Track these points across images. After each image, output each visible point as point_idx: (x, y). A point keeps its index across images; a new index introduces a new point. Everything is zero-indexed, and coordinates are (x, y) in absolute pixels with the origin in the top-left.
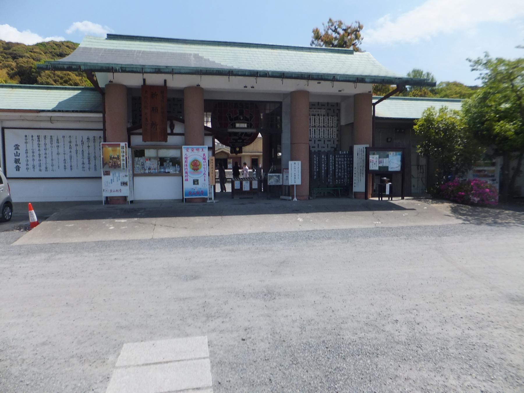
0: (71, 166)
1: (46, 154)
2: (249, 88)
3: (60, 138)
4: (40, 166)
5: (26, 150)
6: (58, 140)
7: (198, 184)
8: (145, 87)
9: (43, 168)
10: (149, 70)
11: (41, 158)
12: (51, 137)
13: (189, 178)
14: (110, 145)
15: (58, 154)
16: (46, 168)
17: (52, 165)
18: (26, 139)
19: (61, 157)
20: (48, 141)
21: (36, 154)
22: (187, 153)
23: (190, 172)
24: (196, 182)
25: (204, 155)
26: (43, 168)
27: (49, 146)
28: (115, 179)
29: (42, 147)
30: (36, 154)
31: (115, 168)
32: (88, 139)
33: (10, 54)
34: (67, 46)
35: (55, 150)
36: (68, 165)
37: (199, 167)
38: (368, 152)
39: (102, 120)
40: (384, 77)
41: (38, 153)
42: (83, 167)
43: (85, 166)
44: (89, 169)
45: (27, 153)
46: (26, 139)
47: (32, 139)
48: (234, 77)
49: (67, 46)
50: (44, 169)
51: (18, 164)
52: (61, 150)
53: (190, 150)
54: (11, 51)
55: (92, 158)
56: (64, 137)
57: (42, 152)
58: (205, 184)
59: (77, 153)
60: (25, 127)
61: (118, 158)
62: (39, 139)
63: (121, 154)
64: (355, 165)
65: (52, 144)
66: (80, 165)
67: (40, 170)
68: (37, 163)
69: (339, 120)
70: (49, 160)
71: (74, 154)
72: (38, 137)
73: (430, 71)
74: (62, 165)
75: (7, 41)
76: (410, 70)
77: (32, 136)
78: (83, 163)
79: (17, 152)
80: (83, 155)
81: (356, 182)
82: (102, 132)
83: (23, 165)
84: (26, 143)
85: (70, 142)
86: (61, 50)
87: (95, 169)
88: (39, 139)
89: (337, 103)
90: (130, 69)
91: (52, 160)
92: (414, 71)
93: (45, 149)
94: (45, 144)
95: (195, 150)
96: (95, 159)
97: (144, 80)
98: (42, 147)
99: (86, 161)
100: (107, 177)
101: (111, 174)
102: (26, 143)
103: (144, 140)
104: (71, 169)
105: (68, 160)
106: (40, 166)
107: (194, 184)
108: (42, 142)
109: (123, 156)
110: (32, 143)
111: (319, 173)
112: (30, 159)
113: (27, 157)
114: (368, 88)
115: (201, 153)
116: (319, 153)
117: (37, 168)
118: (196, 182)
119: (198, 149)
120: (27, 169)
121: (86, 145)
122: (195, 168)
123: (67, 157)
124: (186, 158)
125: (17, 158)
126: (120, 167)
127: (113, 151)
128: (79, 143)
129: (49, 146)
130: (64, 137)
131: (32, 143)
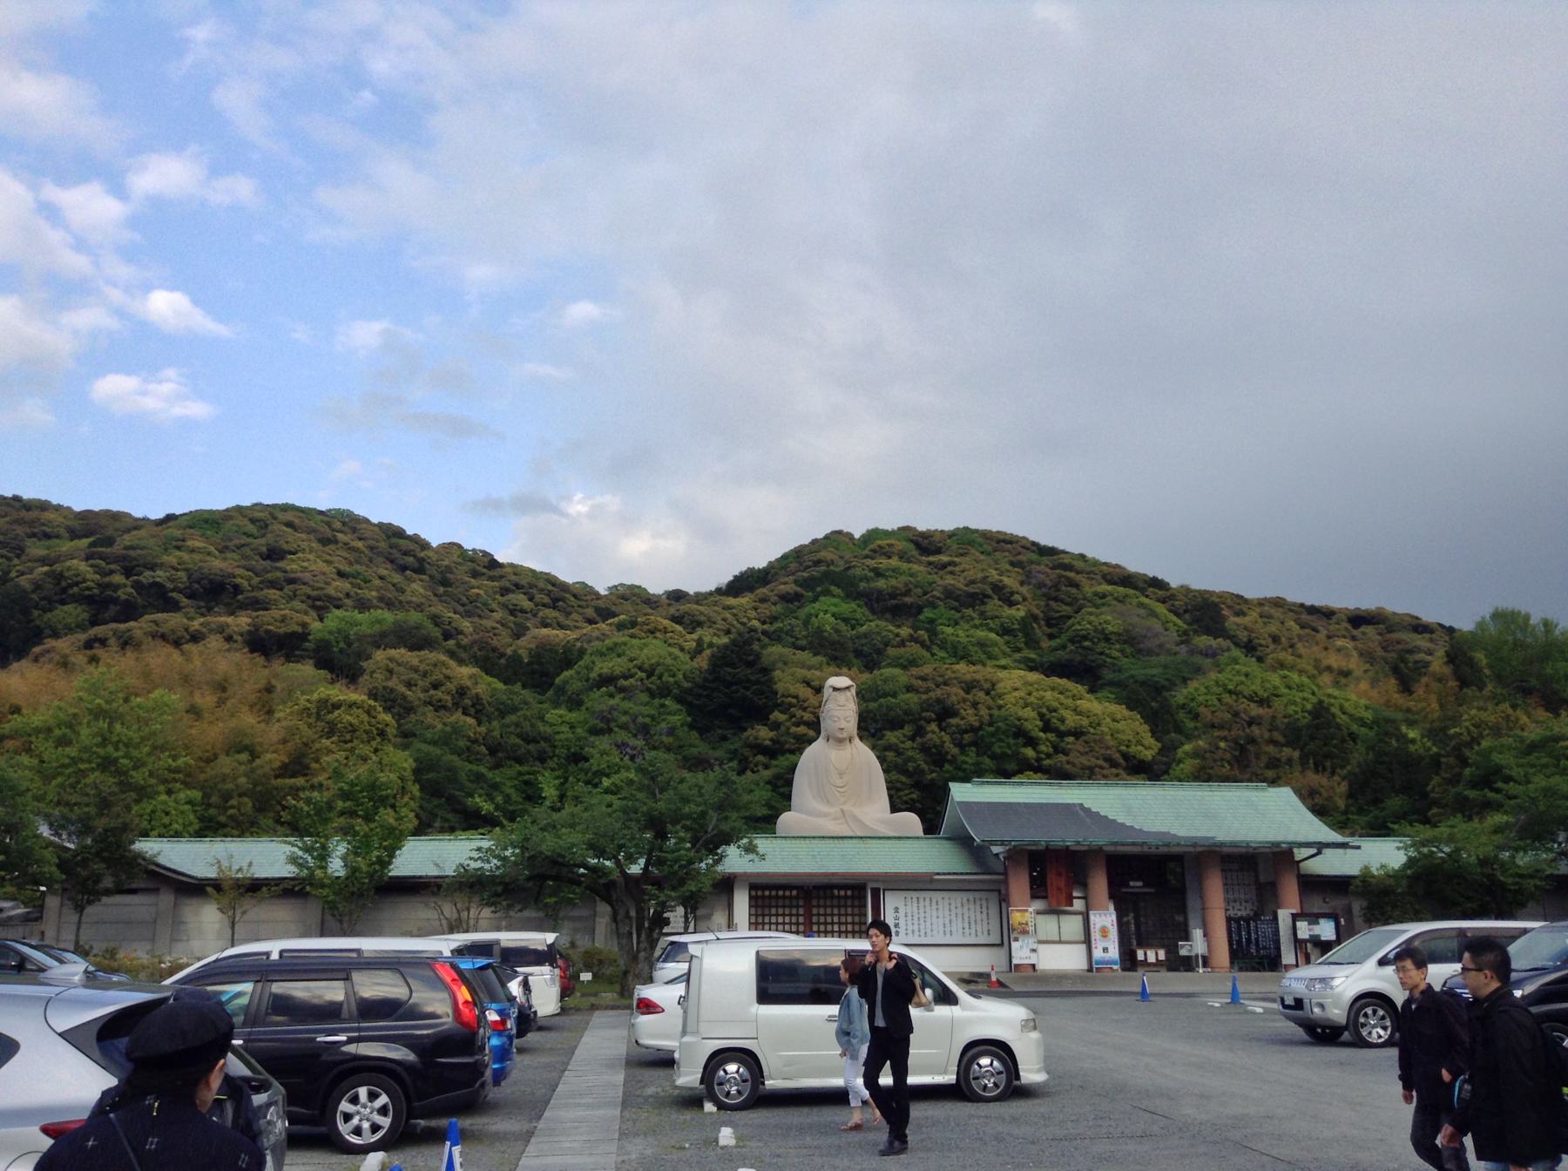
19: (941, 921)
24: (1105, 950)
33: (117, 559)
34: (289, 525)
38: (1295, 917)
49: (289, 525)
54: (117, 549)
64: (1282, 933)
69: (1257, 876)
73: (1552, 616)
75: (78, 508)
76: (1486, 611)
82: (1080, 918)
86: (270, 538)
92: (1497, 616)
111: (1239, 942)
116: (1237, 920)
118: (1105, 950)
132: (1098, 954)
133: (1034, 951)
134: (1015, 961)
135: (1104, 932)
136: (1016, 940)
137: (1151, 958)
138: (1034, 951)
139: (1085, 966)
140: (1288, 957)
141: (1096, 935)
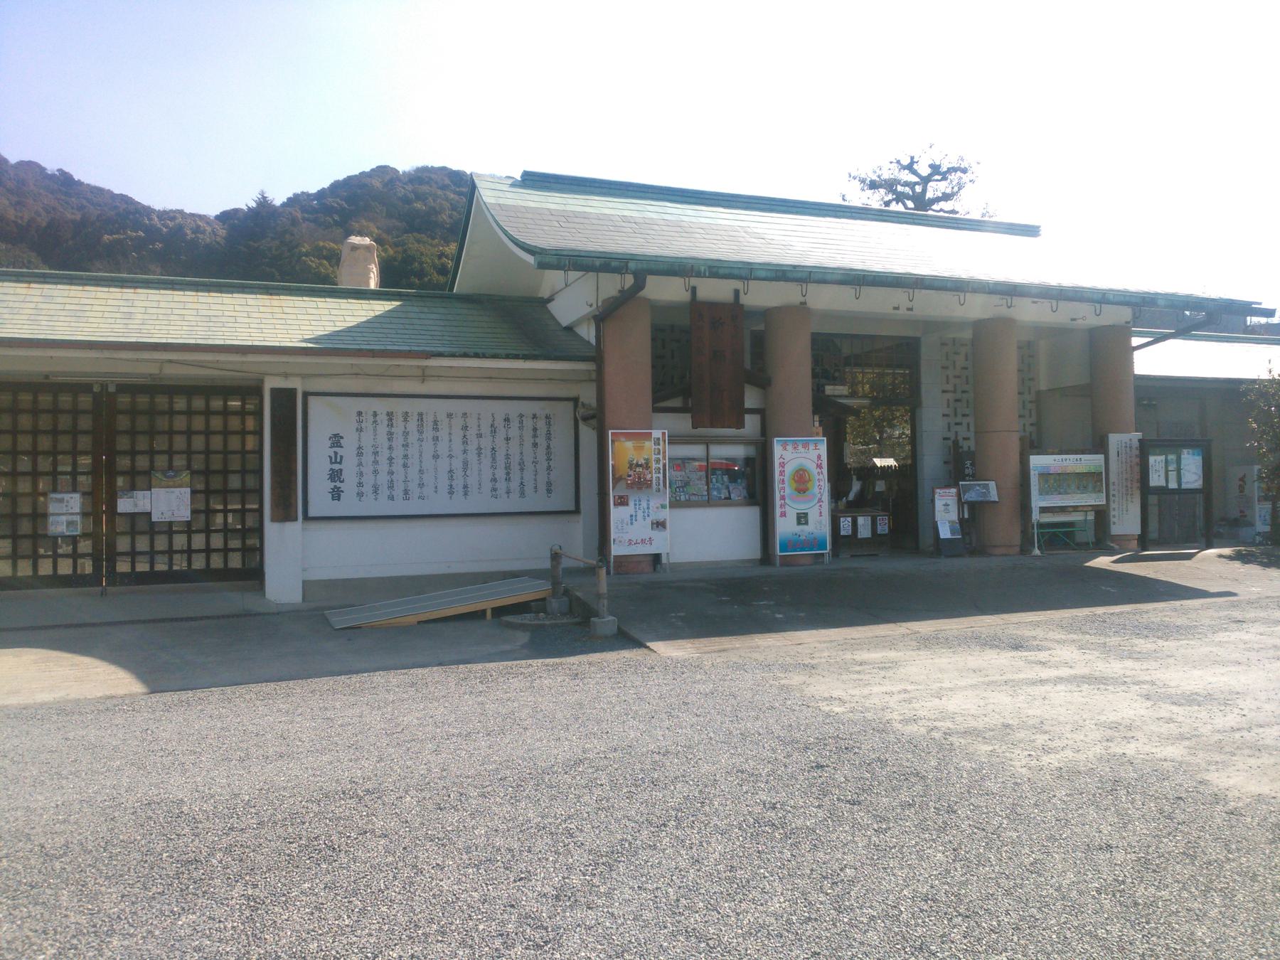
0: (465, 487)
1: (406, 456)
2: (902, 311)
3: (442, 416)
4: (391, 487)
5: (360, 448)
6: (436, 423)
7: (806, 523)
8: (696, 307)
9: (398, 492)
10: (763, 274)
11: (394, 468)
12: (421, 415)
13: (787, 509)
14: (629, 437)
15: (436, 457)
16: (406, 492)
17: (421, 485)
18: (360, 422)
19: (444, 464)
20: (412, 425)
21: (383, 459)
22: (784, 453)
23: (793, 499)
24: (802, 518)
25: (819, 457)
26: (398, 492)
27: (413, 438)
28: (640, 514)
29: (398, 441)
30: (383, 459)
31: (640, 489)
32: (507, 420)
35: (428, 447)
36: (458, 483)
37: (809, 485)
39: (594, 376)
40: (1188, 296)
41: (386, 453)
42: (494, 490)
43: (498, 485)
44: (508, 492)
45: (360, 454)
46: (360, 422)
47: (375, 422)
48: (608, 275)
50: (401, 494)
51: (338, 484)
52: (443, 448)
53: (790, 448)
55: (515, 468)
56: (450, 416)
57: (398, 453)
58: (820, 522)
59: (479, 454)
60: (333, 390)
61: (647, 466)
62: (391, 420)
63: (654, 457)
64: (75, 691)
65: (421, 432)
66: (487, 486)
67: (391, 498)
68: (383, 478)
70: (413, 473)
71: (472, 456)
72: (390, 415)
74: (444, 482)
77: (375, 414)
78: (494, 480)
79: (336, 453)
80: (494, 459)
81: (1116, 513)
83: (349, 486)
84: (360, 430)
85: (465, 428)
87: (522, 494)
88: (391, 420)
89: (1029, 342)
90: (727, 271)
91: (421, 471)
93: (406, 446)
94: (406, 434)
95: (800, 447)
96: (522, 470)
97: (694, 290)
98: (398, 441)
99: (501, 473)
100: (621, 508)
101: (631, 503)
102: (360, 430)
103: (694, 427)
104: (466, 494)
105: (459, 473)
106: (391, 487)
107: (799, 523)
108: (398, 429)
109: (658, 461)
110: (375, 430)
112: (368, 469)
113: (360, 464)
114: (1125, 314)
115: (813, 454)
117: (384, 492)
118: (802, 518)
119: (806, 445)
120: (360, 495)
121: (501, 434)
122: (802, 486)
123: (457, 464)
124: (782, 465)
125: (336, 467)
126: (650, 486)
127: (636, 448)
128: (486, 430)
129: (413, 438)
130: (450, 416)
131: (375, 430)
132: (785, 526)
133: (660, 525)
134: (616, 550)
135: (801, 480)
136: (622, 501)
137: (864, 531)
138: (660, 525)
139: (757, 554)
140: (489, 613)
141: (782, 486)
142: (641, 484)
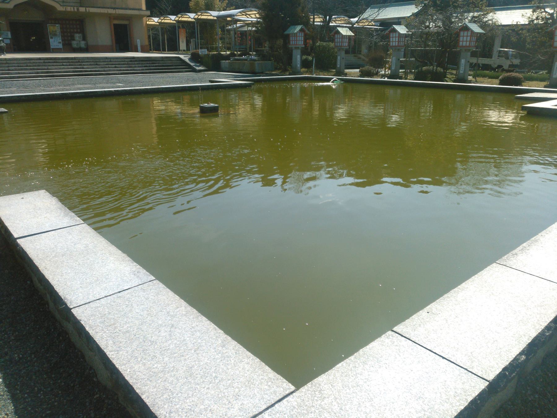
61: (56, 31)
136: (52, 38)
142: (55, 35)
